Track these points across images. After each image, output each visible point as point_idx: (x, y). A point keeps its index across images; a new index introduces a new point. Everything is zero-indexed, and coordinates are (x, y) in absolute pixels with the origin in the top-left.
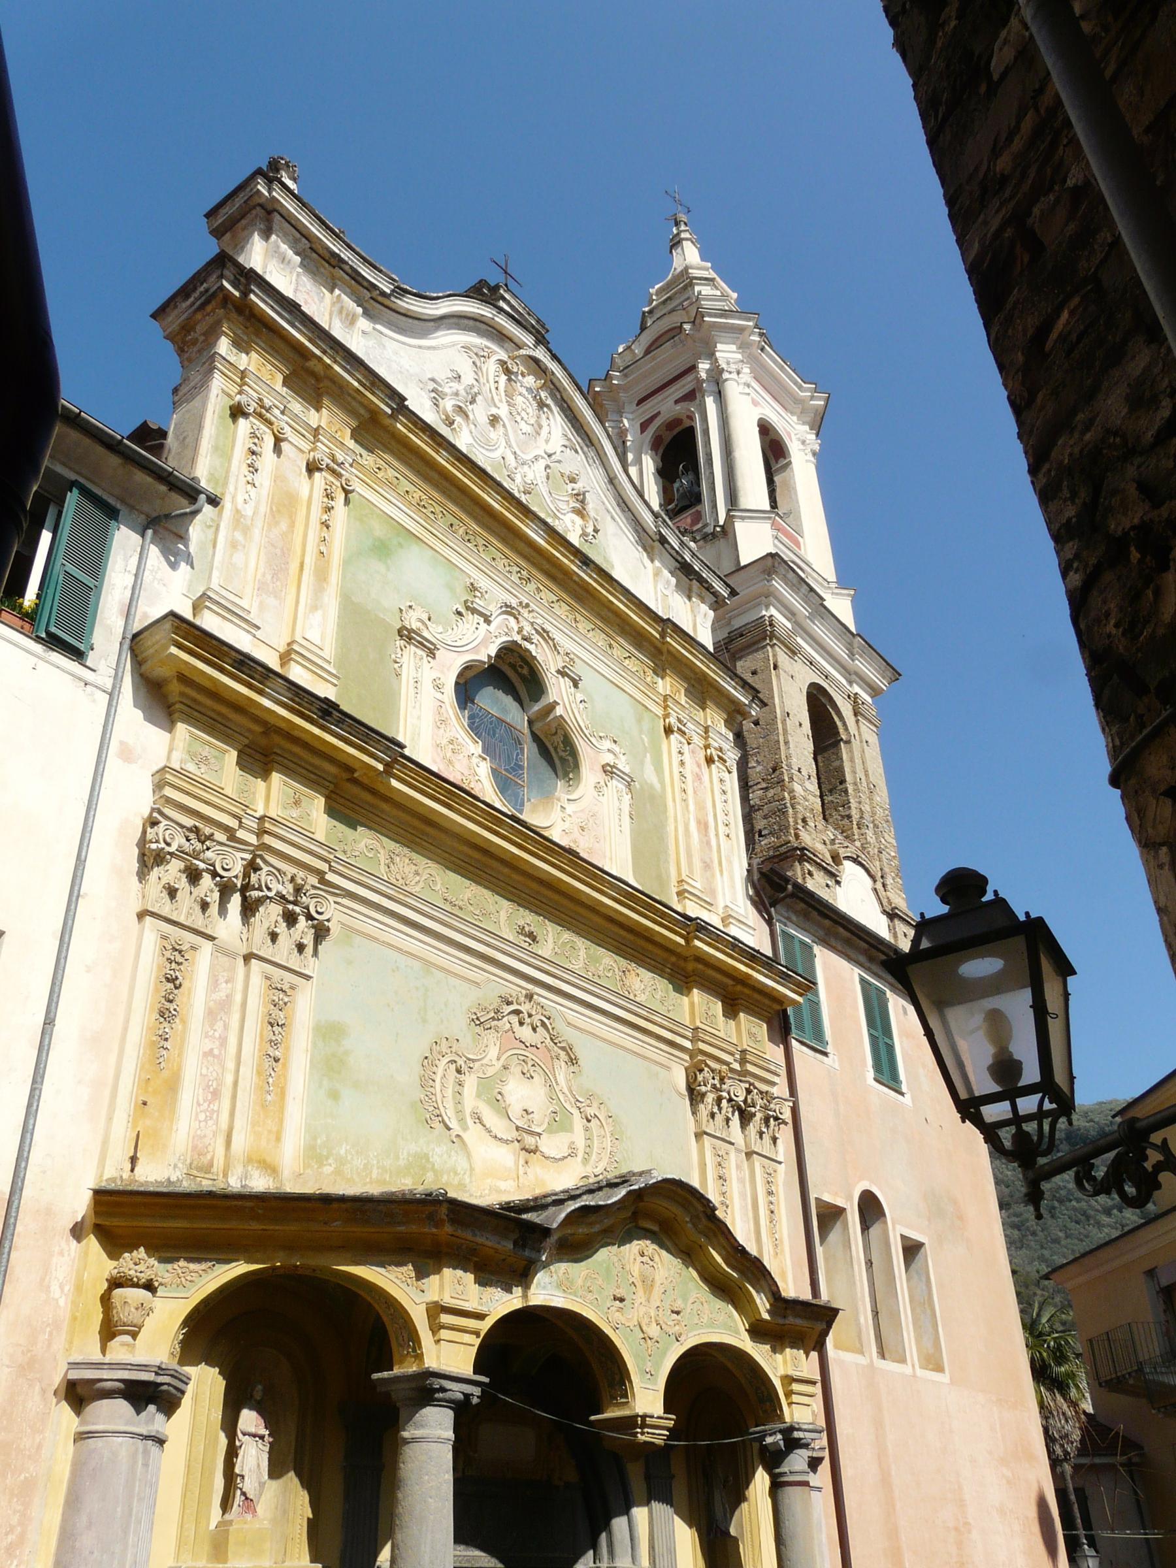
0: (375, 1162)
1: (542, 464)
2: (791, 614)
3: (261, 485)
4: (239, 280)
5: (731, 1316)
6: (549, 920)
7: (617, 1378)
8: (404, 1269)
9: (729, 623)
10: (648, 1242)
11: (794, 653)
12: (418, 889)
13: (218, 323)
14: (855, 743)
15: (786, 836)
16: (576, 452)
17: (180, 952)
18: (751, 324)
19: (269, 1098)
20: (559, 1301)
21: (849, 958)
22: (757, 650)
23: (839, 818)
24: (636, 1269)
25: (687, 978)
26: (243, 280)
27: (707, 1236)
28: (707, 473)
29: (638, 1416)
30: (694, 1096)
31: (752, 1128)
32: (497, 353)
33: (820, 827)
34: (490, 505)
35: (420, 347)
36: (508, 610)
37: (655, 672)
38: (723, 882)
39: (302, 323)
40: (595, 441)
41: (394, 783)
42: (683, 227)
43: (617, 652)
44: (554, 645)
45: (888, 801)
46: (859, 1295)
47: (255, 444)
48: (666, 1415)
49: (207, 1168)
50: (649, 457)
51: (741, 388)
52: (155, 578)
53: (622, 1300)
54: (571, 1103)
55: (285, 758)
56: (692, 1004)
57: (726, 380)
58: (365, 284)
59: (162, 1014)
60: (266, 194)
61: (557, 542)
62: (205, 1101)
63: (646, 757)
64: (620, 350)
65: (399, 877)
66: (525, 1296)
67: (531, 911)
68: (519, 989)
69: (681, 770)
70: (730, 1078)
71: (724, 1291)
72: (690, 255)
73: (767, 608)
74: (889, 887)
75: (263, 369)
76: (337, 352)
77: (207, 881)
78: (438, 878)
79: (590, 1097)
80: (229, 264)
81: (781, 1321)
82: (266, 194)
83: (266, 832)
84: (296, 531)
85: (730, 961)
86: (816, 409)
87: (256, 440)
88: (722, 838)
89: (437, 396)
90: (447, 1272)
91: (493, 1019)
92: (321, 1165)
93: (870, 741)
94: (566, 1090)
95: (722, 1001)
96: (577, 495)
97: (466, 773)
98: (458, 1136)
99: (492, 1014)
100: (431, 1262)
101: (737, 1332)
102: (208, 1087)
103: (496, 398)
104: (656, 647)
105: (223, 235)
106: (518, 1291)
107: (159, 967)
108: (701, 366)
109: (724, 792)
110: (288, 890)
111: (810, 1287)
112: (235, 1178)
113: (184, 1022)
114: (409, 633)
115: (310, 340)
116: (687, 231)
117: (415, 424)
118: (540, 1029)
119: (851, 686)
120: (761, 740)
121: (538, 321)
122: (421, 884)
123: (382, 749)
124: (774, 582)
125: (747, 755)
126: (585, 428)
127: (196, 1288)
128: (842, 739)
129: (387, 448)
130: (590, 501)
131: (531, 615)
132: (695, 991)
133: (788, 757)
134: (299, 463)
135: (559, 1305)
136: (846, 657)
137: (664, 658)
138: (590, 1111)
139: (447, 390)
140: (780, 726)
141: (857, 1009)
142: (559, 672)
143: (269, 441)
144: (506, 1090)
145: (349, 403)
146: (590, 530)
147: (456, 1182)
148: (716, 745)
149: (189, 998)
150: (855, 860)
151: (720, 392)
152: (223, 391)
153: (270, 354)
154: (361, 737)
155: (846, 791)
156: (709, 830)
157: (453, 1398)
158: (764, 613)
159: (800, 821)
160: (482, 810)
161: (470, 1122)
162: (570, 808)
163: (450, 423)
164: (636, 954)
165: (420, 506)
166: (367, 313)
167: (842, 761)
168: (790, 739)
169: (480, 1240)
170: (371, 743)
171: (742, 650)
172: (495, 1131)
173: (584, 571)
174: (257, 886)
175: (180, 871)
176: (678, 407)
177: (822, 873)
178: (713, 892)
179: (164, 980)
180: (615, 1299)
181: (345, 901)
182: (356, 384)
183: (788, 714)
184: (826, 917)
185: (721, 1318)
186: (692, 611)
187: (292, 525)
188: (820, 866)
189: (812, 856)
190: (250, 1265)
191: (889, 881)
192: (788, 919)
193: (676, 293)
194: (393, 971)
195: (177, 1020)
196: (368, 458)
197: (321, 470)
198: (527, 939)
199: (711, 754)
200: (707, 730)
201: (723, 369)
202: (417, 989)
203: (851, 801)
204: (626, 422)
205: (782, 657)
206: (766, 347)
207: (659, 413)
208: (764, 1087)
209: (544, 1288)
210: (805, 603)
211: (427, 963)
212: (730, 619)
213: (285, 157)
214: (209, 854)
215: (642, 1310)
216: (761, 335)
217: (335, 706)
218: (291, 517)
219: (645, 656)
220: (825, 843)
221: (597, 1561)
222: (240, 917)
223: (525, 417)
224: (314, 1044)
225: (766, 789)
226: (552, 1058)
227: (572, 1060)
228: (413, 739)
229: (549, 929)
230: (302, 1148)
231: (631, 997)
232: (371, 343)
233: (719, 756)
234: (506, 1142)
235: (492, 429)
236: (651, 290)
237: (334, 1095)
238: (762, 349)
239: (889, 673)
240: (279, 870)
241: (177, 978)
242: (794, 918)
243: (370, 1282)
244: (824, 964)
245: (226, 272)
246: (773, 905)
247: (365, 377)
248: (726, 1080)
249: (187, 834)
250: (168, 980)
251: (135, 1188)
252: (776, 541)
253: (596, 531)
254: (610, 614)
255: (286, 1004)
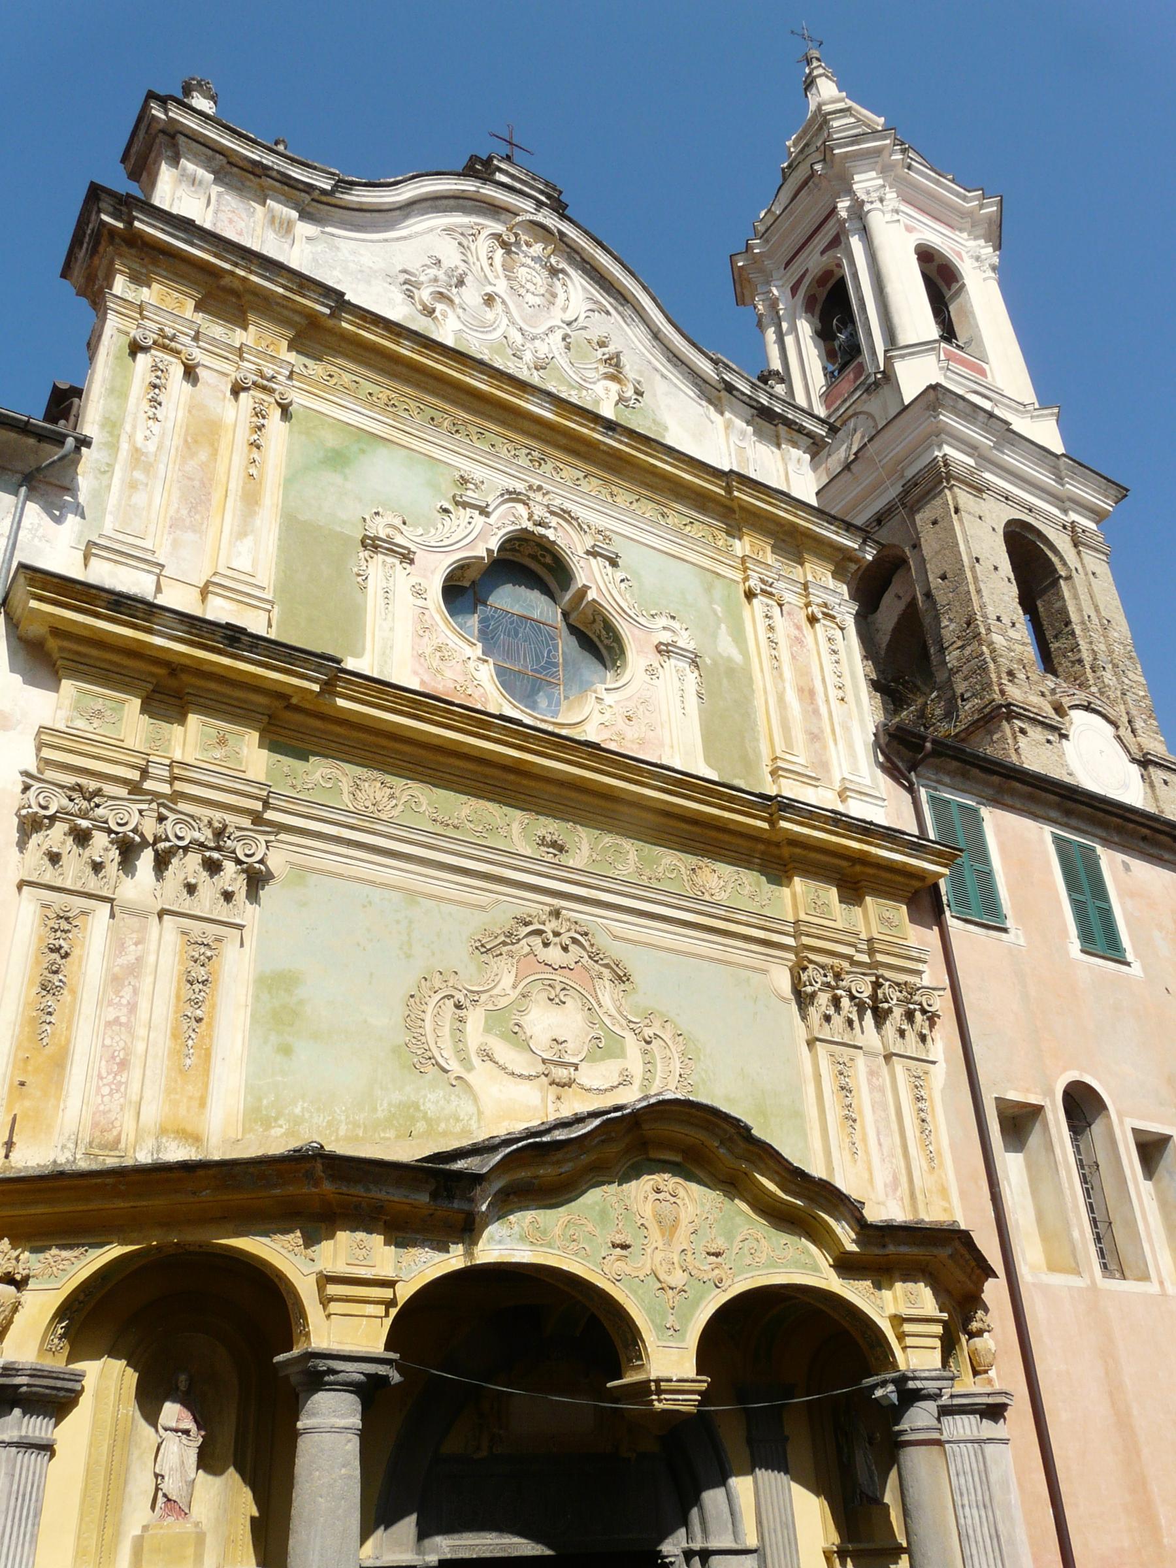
0: (343, 1118)
1: (559, 334)
2: (971, 448)
3: (166, 418)
4: (120, 211)
5: (806, 1251)
6: (581, 825)
7: (629, 1336)
8: (290, 1237)
9: (902, 477)
10: (666, 1176)
11: (980, 491)
12: (395, 813)
13: (112, 263)
14: (1078, 579)
15: (989, 695)
16: (608, 313)
17: (67, 919)
18: (888, 142)
19: (188, 1062)
20: (523, 1255)
21: (1035, 816)
22: (934, 498)
23: (1070, 664)
24: (647, 1210)
25: (785, 866)
26: (124, 209)
27: (753, 1163)
28: (863, 319)
29: (650, 1381)
30: (803, 999)
31: (889, 1028)
32: (487, 227)
33: (1034, 677)
34: (476, 389)
35: (386, 240)
36: (513, 496)
37: (729, 534)
38: (838, 752)
39: (201, 239)
40: (630, 298)
41: (341, 702)
42: (815, 64)
43: (673, 520)
44: (579, 525)
45: (1129, 635)
46: (1069, 1205)
47: (158, 377)
48: (699, 1378)
49: (115, 1144)
50: (804, 321)
51: (888, 217)
52: (34, 536)
53: (625, 1247)
54: (621, 1026)
55: (201, 697)
56: (794, 895)
57: (869, 212)
58: (301, 186)
59: (44, 987)
60: (163, 117)
61: (570, 412)
62: (108, 1074)
63: (720, 628)
64: (762, 215)
65: (368, 804)
66: (469, 1253)
67: (555, 817)
68: (541, 906)
69: (770, 635)
70: (848, 973)
71: (793, 1223)
72: (827, 90)
73: (940, 447)
74: (1139, 732)
75: (168, 299)
76: (250, 261)
77: (100, 840)
78: (422, 799)
79: (649, 1015)
80: (103, 196)
81: (877, 1251)
82: (163, 117)
83: (176, 778)
84: (219, 458)
85: (834, 839)
86: (989, 217)
87: (159, 373)
88: (834, 703)
89: (410, 286)
90: (343, 1236)
91: (504, 943)
92: (268, 1127)
93: (1098, 572)
94: (613, 1012)
95: (838, 887)
96: (610, 359)
97: (461, 679)
98: (459, 1078)
99: (502, 938)
100: (323, 1225)
101: (816, 1269)
102: (113, 1057)
103: (490, 276)
104: (726, 507)
105: (141, 175)
106: (457, 1249)
107: (41, 939)
108: (840, 205)
109: (835, 652)
110: (205, 836)
111: (990, 1203)
112: (144, 1152)
113: (73, 992)
114: (374, 541)
115: (216, 256)
116: (820, 66)
117: (364, 319)
118: (573, 948)
119: (1066, 515)
120: (951, 595)
121: (547, 184)
122: (400, 808)
123: (313, 667)
124: (941, 417)
125: (938, 614)
126: (615, 285)
127: (68, 1277)
128: (1061, 577)
129: (338, 352)
130: (626, 363)
131: (547, 497)
132: (797, 880)
133: (983, 606)
134: (222, 387)
135: (525, 1260)
136: (1053, 483)
137: (737, 517)
138: (648, 1032)
139: (422, 278)
140: (969, 574)
141: (1051, 873)
142: (588, 553)
143: (177, 370)
144: (525, 1021)
145: (279, 314)
146: (630, 393)
147: (458, 1129)
148: (819, 601)
149: (80, 966)
150: (1088, 708)
151: (865, 227)
152: (119, 330)
153: (177, 282)
154: (283, 659)
155: (1073, 633)
156: (817, 697)
157: (348, 1380)
158: (936, 453)
159: (1004, 675)
160: (461, 715)
161: (476, 1061)
162: (609, 698)
163: (429, 312)
164: (709, 847)
165: (390, 404)
166: (305, 215)
167: (1065, 601)
168: (982, 586)
169: (382, 1195)
170: (298, 663)
171: (918, 501)
172: (510, 1068)
173: (611, 437)
174: (164, 837)
175: (65, 834)
176: (825, 258)
177: (1039, 729)
178: (825, 766)
179: (47, 950)
180: (614, 1246)
181: (282, 837)
182: (281, 290)
183: (978, 560)
184: (994, 772)
185: (790, 1252)
186: (783, 459)
187: (215, 453)
188: (1034, 721)
189: (1021, 711)
190: (124, 1247)
191: (1139, 724)
192: (938, 782)
193: (812, 137)
194: (364, 906)
195: (65, 992)
196: (316, 367)
197: (248, 389)
198: (551, 850)
199: (813, 612)
200: (806, 586)
201: (863, 201)
202: (398, 922)
203: (1080, 643)
204: (775, 291)
205: (964, 497)
206: (913, 163)
207: (807, 270)
208: (902, 978)
209: (500, 1242)
210: (987, 432)
211: (412, 895)
212: (903, 470)
213: (196, 76)
214: (100, 811)
215: (659, 1255)
216: (904, 151)
217: (243, 631)
218: (212, 445)
219: (713, 518)
220: (1043, 695)
221: (690, 1541)
222: (153, 873)
223: (532, 288)
224: (257, 998)
225: (962, 647)
226: (592, 978)
227: (620, 977)
228: (384, 653)
229: (583, 835)
230: (241, 1111)
231: (707, 897)
232: (320, 247)
233: (824, 613)
234: (529, 1078)
235: (487, 309)
236: (787, 143)
237: (286, 1050)
238: (909, 167)
239: (1113, 491)
240: (192, 817)
241: (61, 947)
242: (947, 780)
243: (253, 1254)
244: (999, 831)
245: (103, 205)
246: (913, 767)
247: (290, 280)
248: (843, 976)
249: (69, 793)
250: (52, 951)
251: (12, 1175)
252: (949, 374)
253: (639, 393)
254: (658, 481)
255: (210, 958)
